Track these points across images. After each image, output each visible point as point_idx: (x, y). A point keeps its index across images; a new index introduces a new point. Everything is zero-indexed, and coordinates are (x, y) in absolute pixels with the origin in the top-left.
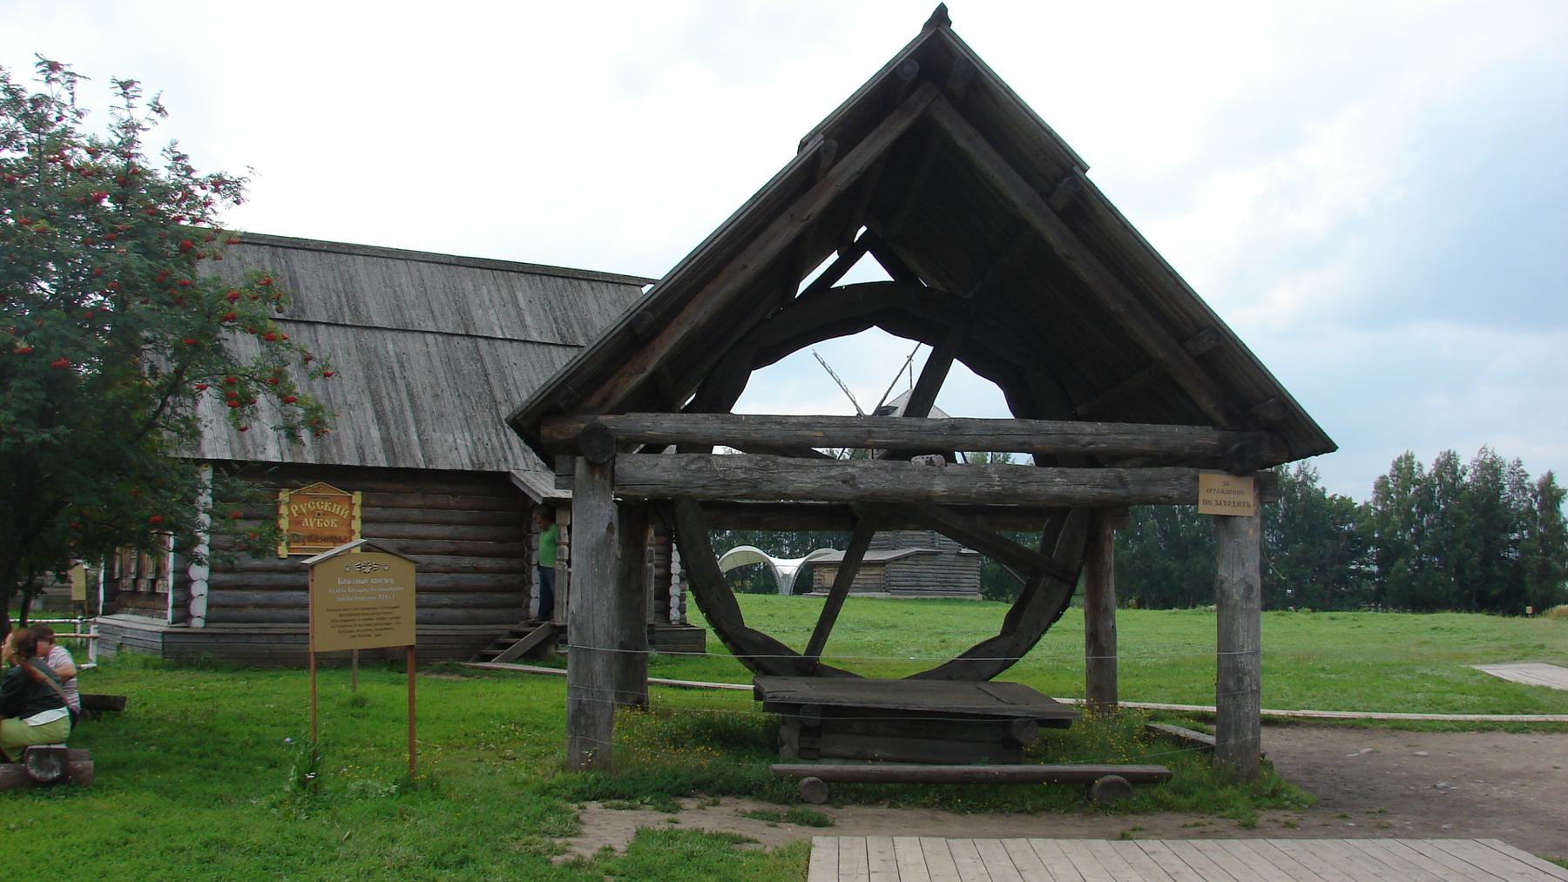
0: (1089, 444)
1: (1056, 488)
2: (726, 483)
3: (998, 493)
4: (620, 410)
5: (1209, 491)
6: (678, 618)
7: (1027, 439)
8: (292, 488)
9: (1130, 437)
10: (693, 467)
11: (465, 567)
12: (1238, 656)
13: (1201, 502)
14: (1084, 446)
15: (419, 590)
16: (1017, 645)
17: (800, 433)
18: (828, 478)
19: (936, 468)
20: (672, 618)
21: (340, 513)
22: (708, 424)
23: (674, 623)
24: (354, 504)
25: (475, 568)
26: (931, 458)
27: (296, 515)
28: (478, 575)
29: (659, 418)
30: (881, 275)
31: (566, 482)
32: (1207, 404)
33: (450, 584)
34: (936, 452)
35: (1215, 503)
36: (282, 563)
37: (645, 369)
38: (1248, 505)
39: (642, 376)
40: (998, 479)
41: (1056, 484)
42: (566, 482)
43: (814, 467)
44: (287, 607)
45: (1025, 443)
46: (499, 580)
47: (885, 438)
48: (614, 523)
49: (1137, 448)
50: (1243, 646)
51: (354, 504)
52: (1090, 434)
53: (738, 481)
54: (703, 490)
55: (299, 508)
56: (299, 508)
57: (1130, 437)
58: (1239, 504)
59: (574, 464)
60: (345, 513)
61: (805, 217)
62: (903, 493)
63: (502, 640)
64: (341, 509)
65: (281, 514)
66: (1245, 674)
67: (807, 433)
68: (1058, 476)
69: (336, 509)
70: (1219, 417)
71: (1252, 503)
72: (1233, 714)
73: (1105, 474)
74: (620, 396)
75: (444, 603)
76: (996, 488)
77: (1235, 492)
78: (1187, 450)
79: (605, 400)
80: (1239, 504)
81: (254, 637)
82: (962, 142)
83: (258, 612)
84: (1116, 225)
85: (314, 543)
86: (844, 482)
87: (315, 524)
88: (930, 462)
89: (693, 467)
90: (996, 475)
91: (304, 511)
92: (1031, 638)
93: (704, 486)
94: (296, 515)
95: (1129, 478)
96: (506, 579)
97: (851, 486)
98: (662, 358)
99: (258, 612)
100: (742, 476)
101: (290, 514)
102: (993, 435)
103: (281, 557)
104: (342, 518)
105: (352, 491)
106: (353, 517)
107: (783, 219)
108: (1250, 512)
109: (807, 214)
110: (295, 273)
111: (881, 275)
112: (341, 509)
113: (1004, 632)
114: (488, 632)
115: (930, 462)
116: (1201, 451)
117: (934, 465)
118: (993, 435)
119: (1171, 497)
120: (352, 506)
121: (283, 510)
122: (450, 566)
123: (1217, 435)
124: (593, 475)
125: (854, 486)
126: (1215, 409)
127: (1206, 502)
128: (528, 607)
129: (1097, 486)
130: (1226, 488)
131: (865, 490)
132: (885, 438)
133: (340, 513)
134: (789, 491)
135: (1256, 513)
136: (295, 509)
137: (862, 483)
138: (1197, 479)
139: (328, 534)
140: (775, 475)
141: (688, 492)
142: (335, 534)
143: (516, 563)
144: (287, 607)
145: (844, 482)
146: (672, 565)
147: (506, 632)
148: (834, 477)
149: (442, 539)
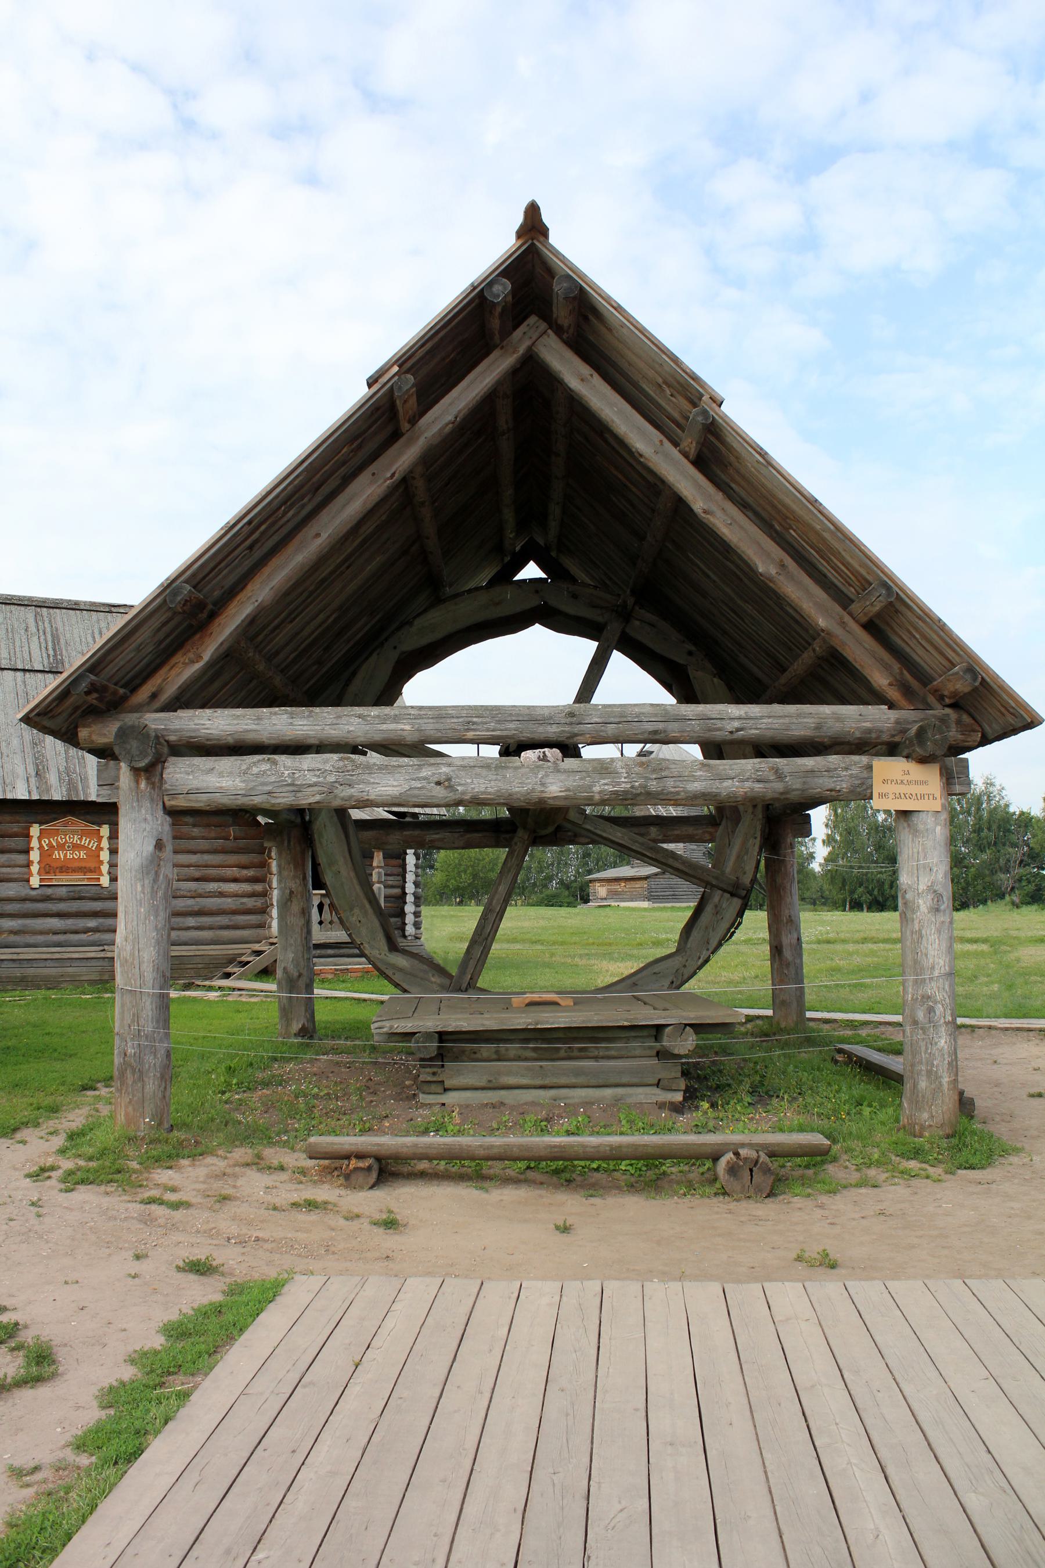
0: (738, 730)
1: (696, 784)
2: (295, 789)
3: (625, 792)
4: (173, 706)
5: (884, 781)
6: (413, 934)
7: (660, 726)
8: (41, 823)
9: (787, 720)
10: (255, 770)
11: (210, 892)
12: (928, 981)
13: (875, 795)
14: (731, 732)
15: (114, 915)
16: (685, 966)
17: (384, 727)
18: (419, 779)
19: (549, 764)
20: (407, 934)
21: (89, 844)
22: (275, 720)
23: (409, 938)
24: (102, 837)
25: (220, 892)
26: (544, 753)
27: (46, 848)
28: (223, 899)
29: (216, 714)
30: (539, 573)
31: (109, 792)
32: (880, 680)
33: (196, 908)
34: (550, 745)
35: (891, 796)
36: (34, 893)
37: (201, 657)
38: (934, 798)
39: (198, 666)
40: (625, 775)
41: (696, 779)
42: (109, 792)
43: (403, 766)
44: (41, 933)
45: (655, 732)
46: (242, 903)
47: (488, 730)
48: (165, 840)
49: (796, 733)
50: (933, 968)
51: (102, 837)
52: (739, 718)
53: (310, 786)
54: (269, 798)
55: (50, 841)
56: (50, 841)
57: (787, 720)
58: (922, 797)
59: (119, 769)
60: (93, 845)
61: (389, 475)
62: (510, 795)
63: (244, 959)
64: (90, 841)
65: (33, 848)
66: (936, 1002)
67: (392, 726)
68: (700, 770)
69: (85, 841)
70: (893, 694)
71: (938, 795)
72: (923, 1049)
73: (757, 766)
74: (170, 691)
75: (191, 925)
76: (623, 785)
77: (916, 782)
78: (858, 734)
79: (154, 696)
80: (922, 797)
81: (6, 962)
82: (573, 383)
83: (12, 938)
84: (758, 462)
85: (64, 874)
86: (438, 783)
87: (66, 855)
88: (544, 758)
89: (255, 770)
90: (624, 771)
91: (55, 844)
92: (699, 958)
93: (269, 793)
94: (46, 848)
95: (786, 770)
96: (250, 903)
97: (446, 788)
98: (222, 644)
99: (12, 938)
100: (315, 779)
101: (41, 848)
102: (619, 723)
103: (33, 887)
104: (91, 849)
105: (100, 824)
106: (102, 849)
107: (364, 478)
108: (937, 805)
109: (392, 471)
110: (57, 630)
111: (539, 573)
112: (90, 841)
113: (679, 950)
114: (231, 952)
115: (544, 758)
116: (874, 735)
117: (549, 761)
118: (619, 723)
119: (839, 791)
120: (100, 839)
121: (35, 843)
122: (195, 891)
123: (893, 715)
124: (137, 782)
125: (451, 788)
126: (890, 684)
127: (881, 795)
128: (270, 927)
129: (747, 780)
130: (906, 778)
131: (463, 793)
132: (488, 730)
133: (89, 844)
134: (372, 797)
135: (943, 806)
136: (45, 843)
137: (460, 785)
138: (869, 768)
139: (76, 864)
140: (354, 778)
141: (252, 800)
142: (83, 865)
143: (259, 887)
144: (41, 933)
145: (438, 783)
146: (407, 885)
147: (249, 951)
148: (425, 778)
149: (188, 866)
